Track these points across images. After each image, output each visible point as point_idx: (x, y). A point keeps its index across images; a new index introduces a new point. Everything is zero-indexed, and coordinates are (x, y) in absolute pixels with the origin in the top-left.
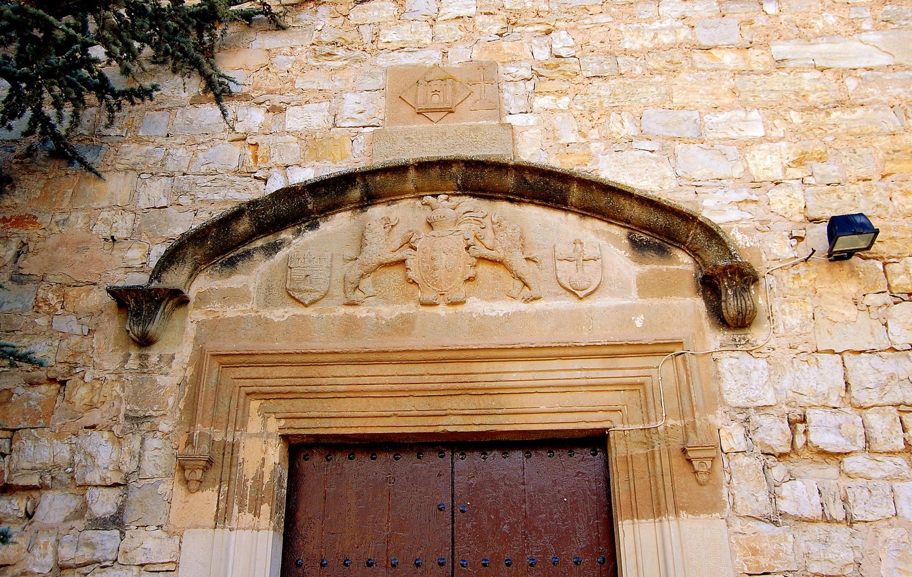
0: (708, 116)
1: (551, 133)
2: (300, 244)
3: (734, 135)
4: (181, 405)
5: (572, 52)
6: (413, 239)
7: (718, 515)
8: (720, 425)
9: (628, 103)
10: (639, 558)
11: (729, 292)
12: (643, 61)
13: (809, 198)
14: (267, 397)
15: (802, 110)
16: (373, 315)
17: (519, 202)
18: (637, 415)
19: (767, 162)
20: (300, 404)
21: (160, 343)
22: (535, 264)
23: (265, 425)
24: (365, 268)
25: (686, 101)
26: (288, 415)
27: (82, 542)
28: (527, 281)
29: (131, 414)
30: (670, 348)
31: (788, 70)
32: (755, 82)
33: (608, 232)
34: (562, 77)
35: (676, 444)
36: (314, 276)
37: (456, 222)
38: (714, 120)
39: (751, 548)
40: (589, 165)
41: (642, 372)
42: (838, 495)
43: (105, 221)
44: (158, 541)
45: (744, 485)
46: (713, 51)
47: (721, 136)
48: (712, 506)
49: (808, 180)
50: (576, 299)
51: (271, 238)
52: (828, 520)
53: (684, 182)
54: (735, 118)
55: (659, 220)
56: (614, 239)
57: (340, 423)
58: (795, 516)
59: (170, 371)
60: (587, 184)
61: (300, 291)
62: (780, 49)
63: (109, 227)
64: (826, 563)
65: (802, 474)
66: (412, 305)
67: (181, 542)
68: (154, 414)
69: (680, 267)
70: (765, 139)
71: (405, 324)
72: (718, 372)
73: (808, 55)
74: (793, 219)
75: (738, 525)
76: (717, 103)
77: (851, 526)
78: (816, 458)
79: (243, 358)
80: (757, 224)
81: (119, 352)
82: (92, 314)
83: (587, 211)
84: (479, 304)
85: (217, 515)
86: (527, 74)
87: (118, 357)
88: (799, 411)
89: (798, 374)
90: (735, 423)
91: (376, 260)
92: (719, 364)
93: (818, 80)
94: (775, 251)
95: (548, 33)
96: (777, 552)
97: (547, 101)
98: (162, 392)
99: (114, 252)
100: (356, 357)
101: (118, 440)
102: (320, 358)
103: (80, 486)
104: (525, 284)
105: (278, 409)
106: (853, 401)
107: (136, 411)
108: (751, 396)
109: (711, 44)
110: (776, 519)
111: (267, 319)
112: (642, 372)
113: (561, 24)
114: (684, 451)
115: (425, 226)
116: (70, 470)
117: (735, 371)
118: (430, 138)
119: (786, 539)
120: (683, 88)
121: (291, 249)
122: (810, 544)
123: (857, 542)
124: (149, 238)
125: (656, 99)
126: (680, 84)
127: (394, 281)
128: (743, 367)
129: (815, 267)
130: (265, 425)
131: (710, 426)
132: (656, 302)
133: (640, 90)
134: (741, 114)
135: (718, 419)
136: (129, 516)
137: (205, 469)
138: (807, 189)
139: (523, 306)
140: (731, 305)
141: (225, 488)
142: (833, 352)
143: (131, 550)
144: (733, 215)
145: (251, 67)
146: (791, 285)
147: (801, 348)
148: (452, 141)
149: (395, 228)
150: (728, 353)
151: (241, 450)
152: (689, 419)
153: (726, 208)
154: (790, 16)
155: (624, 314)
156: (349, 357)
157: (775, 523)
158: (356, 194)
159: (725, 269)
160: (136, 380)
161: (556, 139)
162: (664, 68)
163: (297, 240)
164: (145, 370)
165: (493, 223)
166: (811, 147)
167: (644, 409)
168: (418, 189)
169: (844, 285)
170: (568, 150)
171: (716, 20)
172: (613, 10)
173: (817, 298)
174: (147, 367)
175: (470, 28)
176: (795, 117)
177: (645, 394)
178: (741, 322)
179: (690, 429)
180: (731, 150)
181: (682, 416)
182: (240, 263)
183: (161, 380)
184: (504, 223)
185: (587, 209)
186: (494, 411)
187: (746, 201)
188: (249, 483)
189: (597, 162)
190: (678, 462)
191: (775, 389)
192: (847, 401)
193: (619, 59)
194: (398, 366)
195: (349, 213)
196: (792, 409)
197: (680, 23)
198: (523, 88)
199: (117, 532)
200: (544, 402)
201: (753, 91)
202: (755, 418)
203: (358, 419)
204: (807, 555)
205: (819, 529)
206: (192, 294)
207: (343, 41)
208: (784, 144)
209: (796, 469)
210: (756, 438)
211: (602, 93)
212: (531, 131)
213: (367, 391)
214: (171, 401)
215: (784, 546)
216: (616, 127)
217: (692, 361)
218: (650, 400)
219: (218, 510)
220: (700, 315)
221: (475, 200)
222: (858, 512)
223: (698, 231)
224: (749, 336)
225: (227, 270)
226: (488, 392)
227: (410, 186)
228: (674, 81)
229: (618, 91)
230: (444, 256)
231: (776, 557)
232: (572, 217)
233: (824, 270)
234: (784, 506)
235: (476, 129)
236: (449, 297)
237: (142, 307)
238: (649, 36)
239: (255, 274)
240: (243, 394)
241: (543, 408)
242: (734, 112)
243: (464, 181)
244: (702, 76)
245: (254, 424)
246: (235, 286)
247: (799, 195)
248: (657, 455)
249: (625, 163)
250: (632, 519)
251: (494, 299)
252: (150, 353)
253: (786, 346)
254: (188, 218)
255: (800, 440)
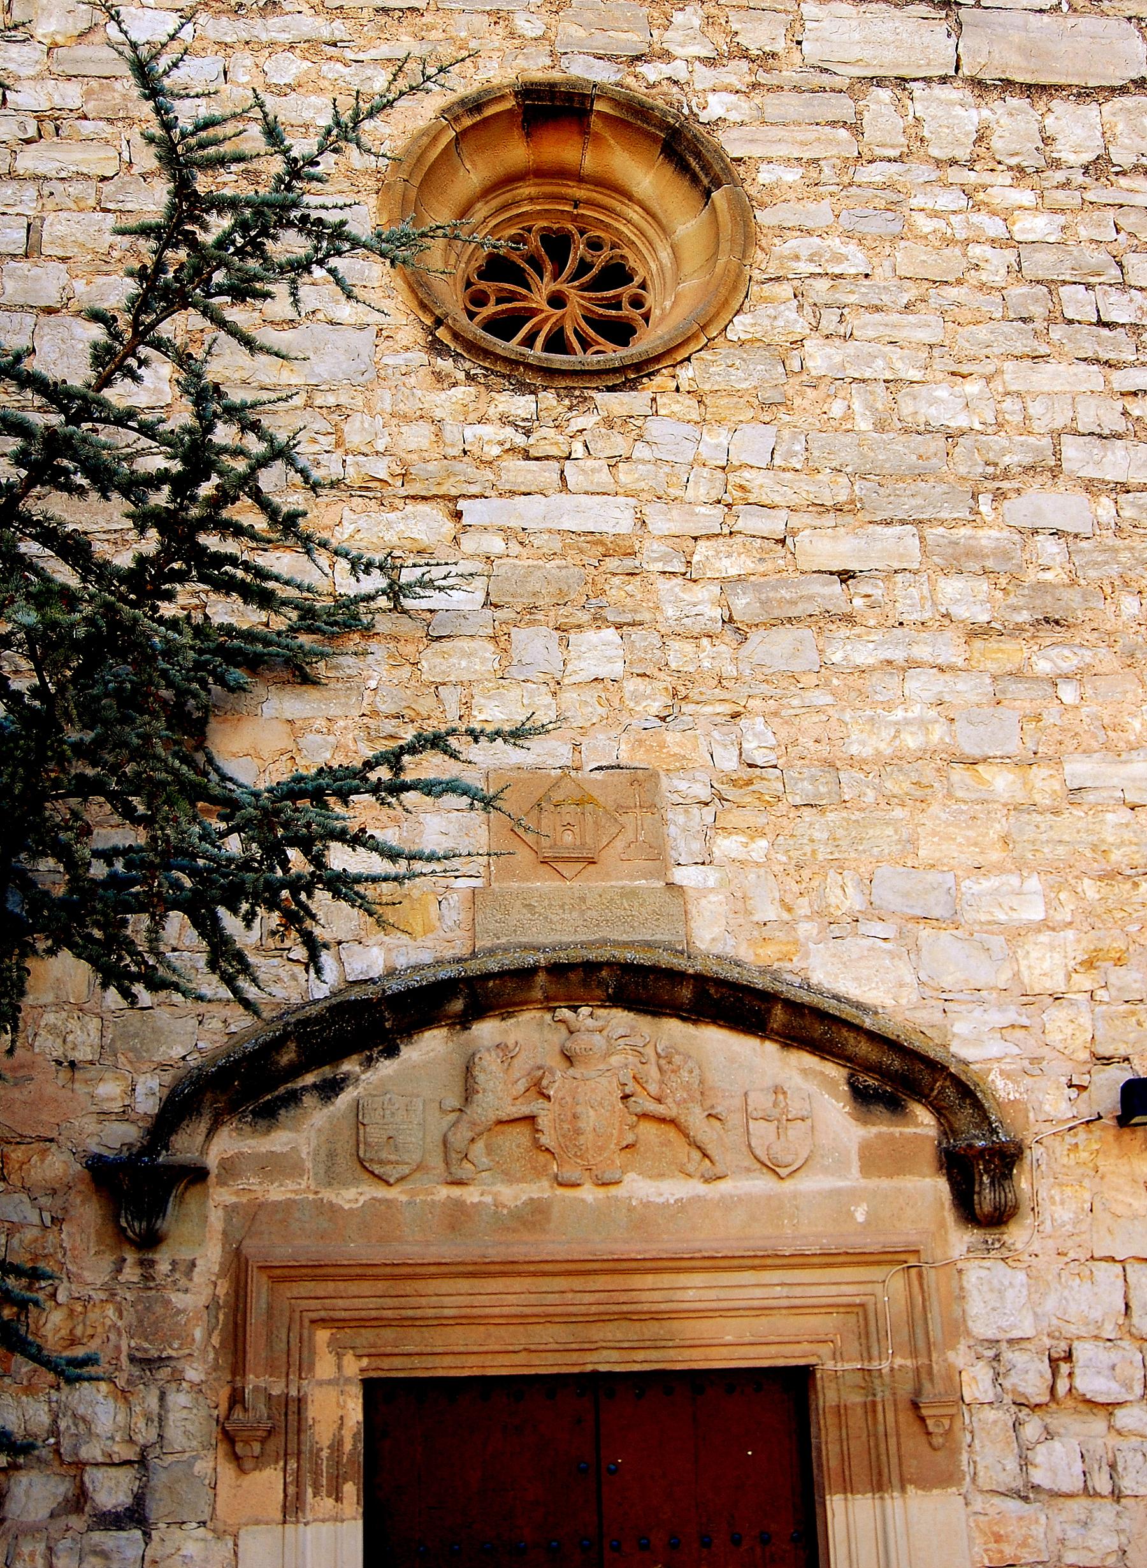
0: (967, 883)
1: (741, 902)
2: (373, 1080)
3: (1002, 917)
4: (215, 1340)
5: (772, 758)
6: (544, 1082)
7: (954, 1489)
8: (961, 1366)
9: (853, 855)
10: (853, 1546)
11: (985, 1178)
12: (877, 781)
13: (1099, 1024)
14: (340, 1324)
15: (1100, 878)
16: (488, 1199)
17: (695, 1022)
18: (853, 1347)
19: (1046, 963)
20: (389, 1334)
21: (170, 1241)
22: (718, 1123)
23: (339, 1367)
24: (478, 1129)
25: (937, 855)
26: (373, 1351)
27: (87, 1549)
28: (709, 1152)
29: (139, 1355)
30: (903, 1257)
31: (1085, 808)
32: (1037, 827)
33: (822, 1073)
34: (757, 803)
35: (905, 1389)
36: (400, 1139)
37: (608, 1054)
38: (976, 888)
39: (993, 1534)
40: (795, 959)
41: (862, 1289)
42: (1104, 1461)
43: (52, 1029)
44: (202, 1544)
45: (989, 1453)
46: (979, 767)
47: (984, 918)
48: (947, 1478)
49: (1101, 994)
50: (774, 1178)
51: (327, 1071)
52: (1088, 1492)
53: (928, 993)
54: (1005, 888)
55: (895, 1063)
56: (828, 1083)
57: (448, 1361)
58: (1050, 1490)
59: (190, 1285)
60: (794, 1007)
61: (381, 1162)
62: (1078, 769)
63: (59, 1041)
64: (1085, 1552)
65: (1062, 1431)
66: (545, 1184)
67: (236, 1545)
68: (174, 1354)
69: (918, 1130)
70: (1046, 925)
71: (535, 1215)
72: (962, 1288)
73: (1115, 781)
74: (1074, 1057)
75: (978, 1503)
76: (980, 860)
77: (1118, 1502)
78: (1081, 1407)
79: (304, 1271)
80: (1026, 1063)
81: (106, 1256)
82: (54, 1192)
83: (791, 1039)
84: (641, 1184)
85: (284, 1506)
86: (705, 794)
87: (107, 1263)
88: (1063, 1345)
89: (1066, 1293)
90: (981, 1363)
91: (492, 1117)
92: (964, 1277)
93: (1127, 825)
94: (1047, 1107)
95: (735, 716)
96: (1026, 1538)
97: (734, 846)
98: (182, 1319)
99: (77, 1086)
100: (471, 1268)
101: (124, 1395)
102: (418, 1270)
103: (70, 1464)
104: (705, 1155)
105: (358, 1342)
106: (1133, 1330)
107: (146, 1350)
108: (1004, 1324)
109: (976, 752)
110: (1028, 1493)
111: (330, 1203)
112: (862, 1289)
113: (754, 704)
114: (915, 1406)
115: (559, 1058)
116: (52, 1440)
117: (985, 1288)
118: (562, 907)
119: (1037, 1521)
120: (934, 833)
121: (360, 1089)
122: (1066, 1526)
123: (1125, 1523)
124: (131, 1062)
125: (894, 848)
126: (929, 824)
127: (518, 1146)
128: (995, 1281)
129: (1098, 1133)
130: (339, 1367)
131: (950, 1367)
132: (885, 1183)
133: (871, 832)
134: (1014, 880)
135: (959, 1357)
136: (156, 1509)
137: (263, 1441)
138: (1097, 1009)
139: (698, 1188)
140: (986, 1199)
141: (293, 1465)
142: (1113, 1259)
143: (163, 1559)
144: (994, 1048)
145: (266, 756)
146: (1065, 1160)
147: (1072, 1255)
148: (594, 913)
149: (515, 1060)
150: (977, 1262)
151: (310, 1406)
152: (923, 1361)
153: (985, 1038)
154: (1095, 708)
155: (841, 1200)
156: (461, 1269)
157: (1026, 1499)
158: (458, 1005)
159: (983, 1150)
160: (139, 1299)
161: (749, 913)
162: (907, 794)
163: (368, 1074)
164: (152, 1284)
165: (659, 1056)
166: (1108, 941)
167: (863, 1341)
168: (548, 999)
169: (1135, 1161)
170: (766, 932)
171: (987, 710)
172: (835, 682)
173: (1097, 1180)
174: (154, 1279)
175: (616, 704)
176: (1090, 889)
177: (866, 1319)
178: (999, 1218)
179: (924, 1375)
180: (997, 942)
181: (914, 1353)
182: (282, 1112)
183: (178, 1299)
184: (677, 1059)
185: (793, 1039)
186: (663, 1343)
187: (1013, 1026)
188: (325, 1454)
189: (807, 955)
190: (906, 1417)
191: (1035, 1314)
192: (1125, 1329)
193: (842, 775)
194: (529, 1280)
195: (444, 1032)
196: (1055, 1342)
197: (932, 713)
198: (698, 819)
199: (138, 1534)
200: (730, 1330)
201: (1034, 842)
202: (1008, 1355)
203: (473, 1357)
204: (1062, 1541)
205: (1078, 1507)
206: (212, 1161)
207: (413, 713)
208: (1070, 934)
209: (1054, 1423)
210: (1007, 1384)
211: (817, 835)
212: (712, 898)
213: (486, 1317)
214: (198, 1333)
215: (1035, 1527)
216: (834, 897)
217: (931, 1276)
218: (873, 1329)
219: (286, 1496)
220: (942, 1204)
221: (631, 1015)
222: (1127, 1484)
223: (948, 1083)
224: (1005, 1237)
225: (262, 1123)
226: (655, 1316)
227: (538, 994)
228: (921, 818)
229: (840, 833)
230: (592, 1113)
231: (1024, 1544)
232: (771, 1047)
233: (1111, 1138)
234: (1038, 1476)
235: (632, 894)
236: (599, 1173)
237: (139, 1190)
238: (887, 733)
239: (307, 1131)
240: (306, 1323)
241: (729, 1338)
242: (1004, 878)
243: (619, 988)
244: (962, 812)
245: (325, 1367)
246: (277, 1149)
247: (1085, 1020)
248: (880, 1408)
249: (846, 958)
250: (845, 1492)
251: (661, 1176)
252: (157, 1257)
253: (1053, 1252)
254: (190, 1029)
255: (1062, 1387)
